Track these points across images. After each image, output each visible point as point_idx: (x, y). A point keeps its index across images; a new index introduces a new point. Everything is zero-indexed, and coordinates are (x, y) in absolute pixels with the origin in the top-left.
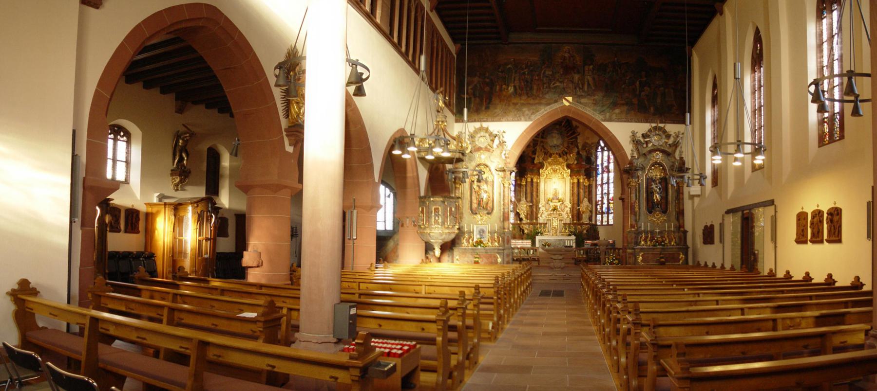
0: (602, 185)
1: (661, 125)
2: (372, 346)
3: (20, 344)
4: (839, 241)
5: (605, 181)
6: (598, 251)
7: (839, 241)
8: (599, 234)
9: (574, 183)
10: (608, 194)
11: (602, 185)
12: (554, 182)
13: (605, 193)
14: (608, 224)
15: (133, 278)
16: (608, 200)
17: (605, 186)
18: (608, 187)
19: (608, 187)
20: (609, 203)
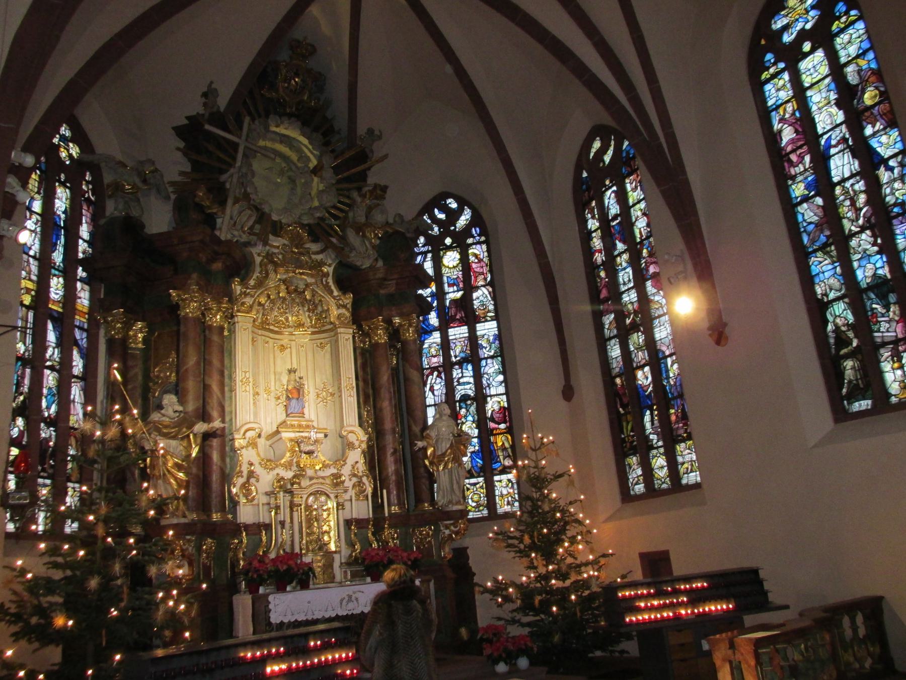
0: (447, 367)
1: (607, 327)
2: (630, 323)
3: (703, 314)
4: (180, 131)
5: (457, 351)
6: (530, 509)
7: (180, 131)
8: (468, 558)
9: (375, 346)
10: (480, 398)
11: (447, 367)
12: (283, 348)
13: (465, 398)
14: (493, 515)
15: (91, 432)
16: (481, 421)
17: (465, 378)
18: (478, 376)
19: (478, 376)
20: (485, 434)
